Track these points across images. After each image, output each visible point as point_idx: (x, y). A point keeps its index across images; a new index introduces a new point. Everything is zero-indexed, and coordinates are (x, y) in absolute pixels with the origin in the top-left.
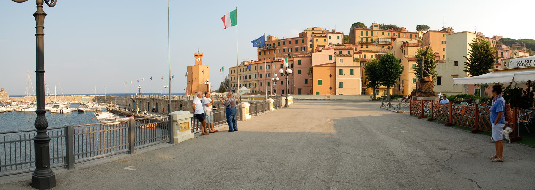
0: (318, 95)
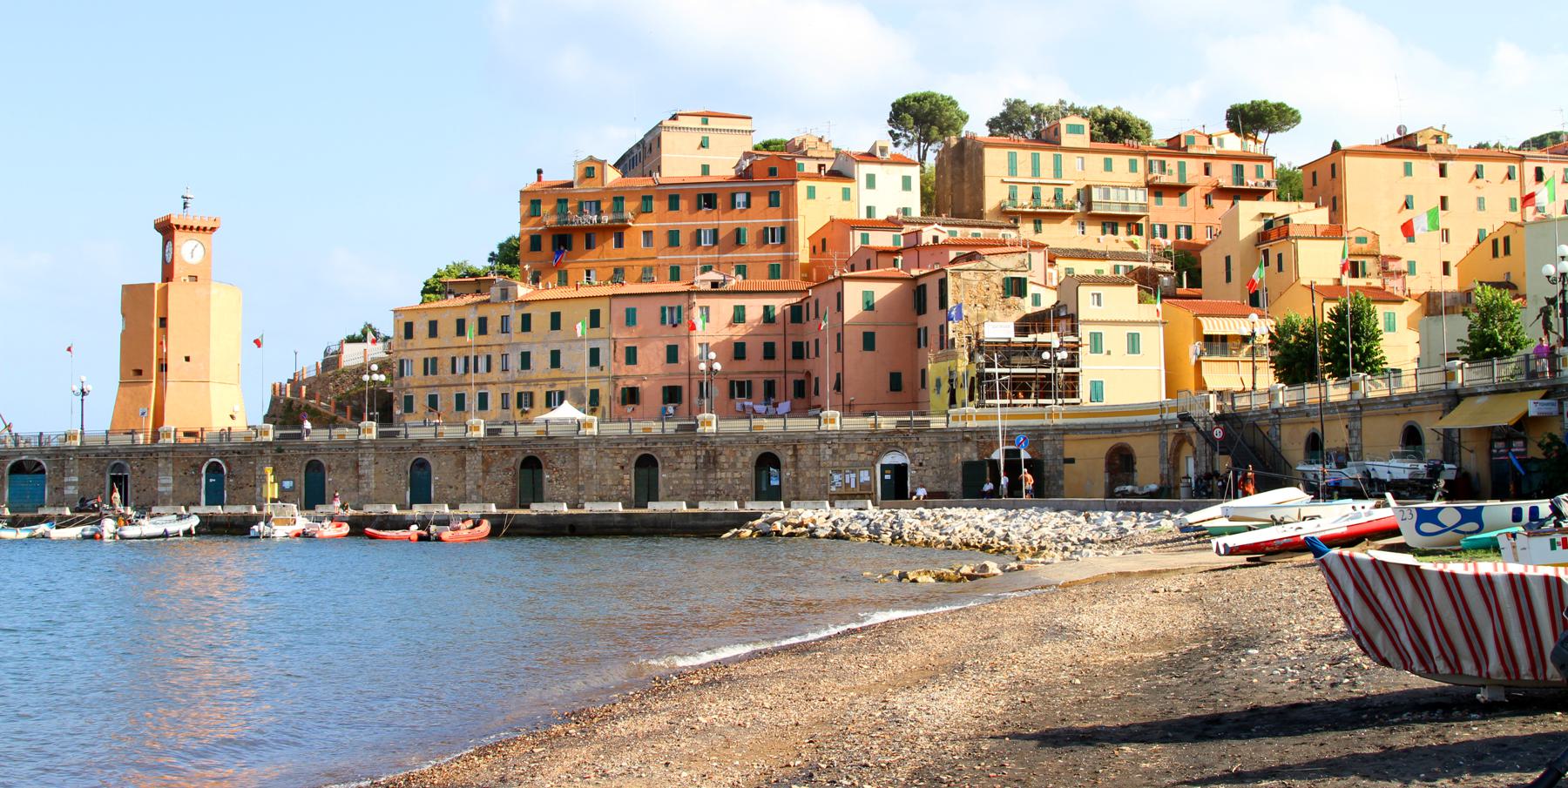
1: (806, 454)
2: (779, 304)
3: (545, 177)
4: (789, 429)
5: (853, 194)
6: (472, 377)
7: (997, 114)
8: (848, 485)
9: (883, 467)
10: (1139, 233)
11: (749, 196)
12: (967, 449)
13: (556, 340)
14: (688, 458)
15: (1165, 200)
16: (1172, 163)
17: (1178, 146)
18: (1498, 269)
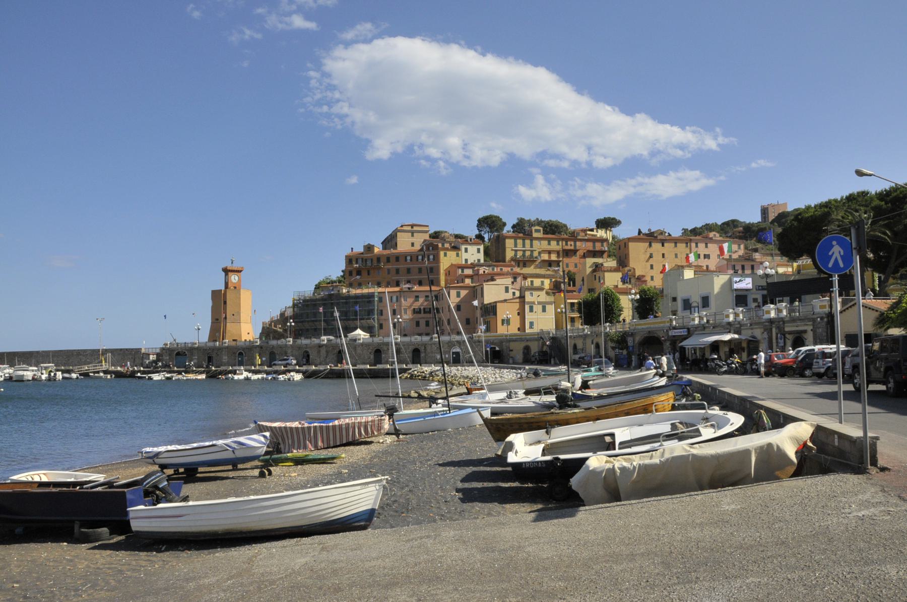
0: (702, 346)
3: (354, 250)
5: (460, 255)
7: (515, 223)
9: (453, 353)
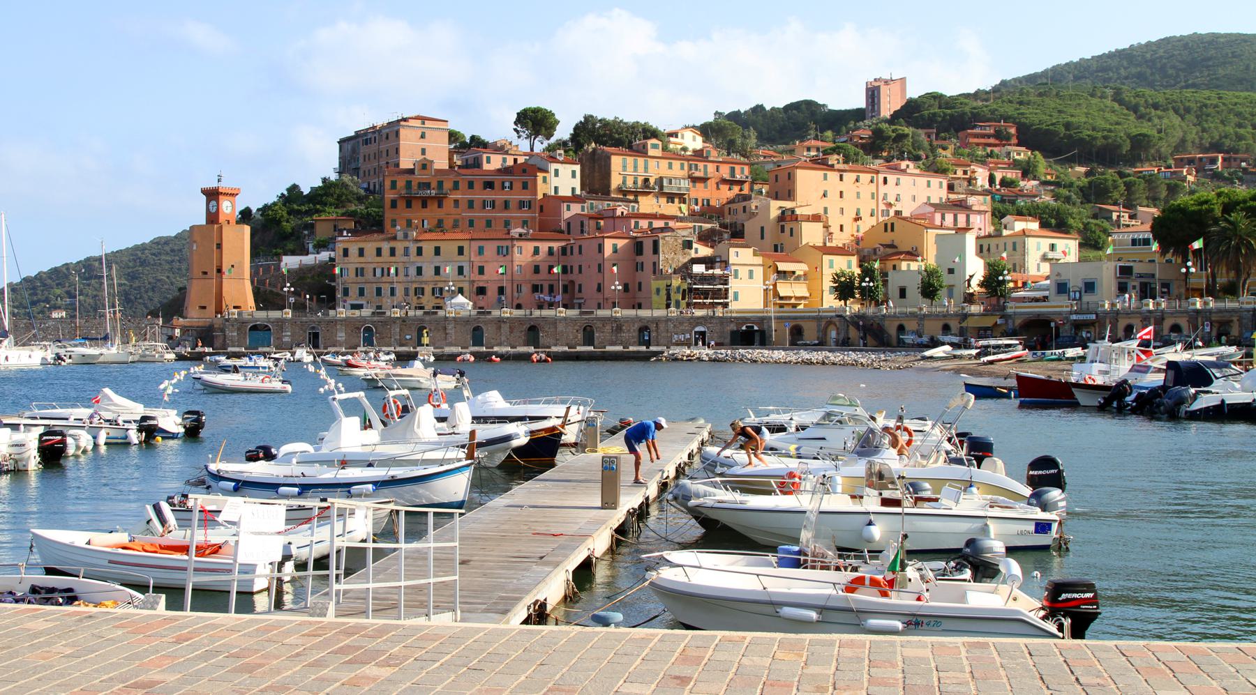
1: (662, 326)
2: (556, 245)
4: (654, 315)
6: (385, 279)
8: (680, 340)
10: (684, 203)
11: (511, 183)
12: (732, 325)
13: (419, 261)
14: (608, 327)
15: (697, 184)
16: (701, 165)
17: (701, 155)
18: (888, 238)
